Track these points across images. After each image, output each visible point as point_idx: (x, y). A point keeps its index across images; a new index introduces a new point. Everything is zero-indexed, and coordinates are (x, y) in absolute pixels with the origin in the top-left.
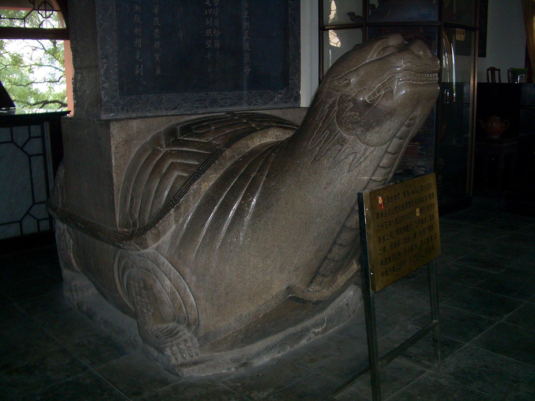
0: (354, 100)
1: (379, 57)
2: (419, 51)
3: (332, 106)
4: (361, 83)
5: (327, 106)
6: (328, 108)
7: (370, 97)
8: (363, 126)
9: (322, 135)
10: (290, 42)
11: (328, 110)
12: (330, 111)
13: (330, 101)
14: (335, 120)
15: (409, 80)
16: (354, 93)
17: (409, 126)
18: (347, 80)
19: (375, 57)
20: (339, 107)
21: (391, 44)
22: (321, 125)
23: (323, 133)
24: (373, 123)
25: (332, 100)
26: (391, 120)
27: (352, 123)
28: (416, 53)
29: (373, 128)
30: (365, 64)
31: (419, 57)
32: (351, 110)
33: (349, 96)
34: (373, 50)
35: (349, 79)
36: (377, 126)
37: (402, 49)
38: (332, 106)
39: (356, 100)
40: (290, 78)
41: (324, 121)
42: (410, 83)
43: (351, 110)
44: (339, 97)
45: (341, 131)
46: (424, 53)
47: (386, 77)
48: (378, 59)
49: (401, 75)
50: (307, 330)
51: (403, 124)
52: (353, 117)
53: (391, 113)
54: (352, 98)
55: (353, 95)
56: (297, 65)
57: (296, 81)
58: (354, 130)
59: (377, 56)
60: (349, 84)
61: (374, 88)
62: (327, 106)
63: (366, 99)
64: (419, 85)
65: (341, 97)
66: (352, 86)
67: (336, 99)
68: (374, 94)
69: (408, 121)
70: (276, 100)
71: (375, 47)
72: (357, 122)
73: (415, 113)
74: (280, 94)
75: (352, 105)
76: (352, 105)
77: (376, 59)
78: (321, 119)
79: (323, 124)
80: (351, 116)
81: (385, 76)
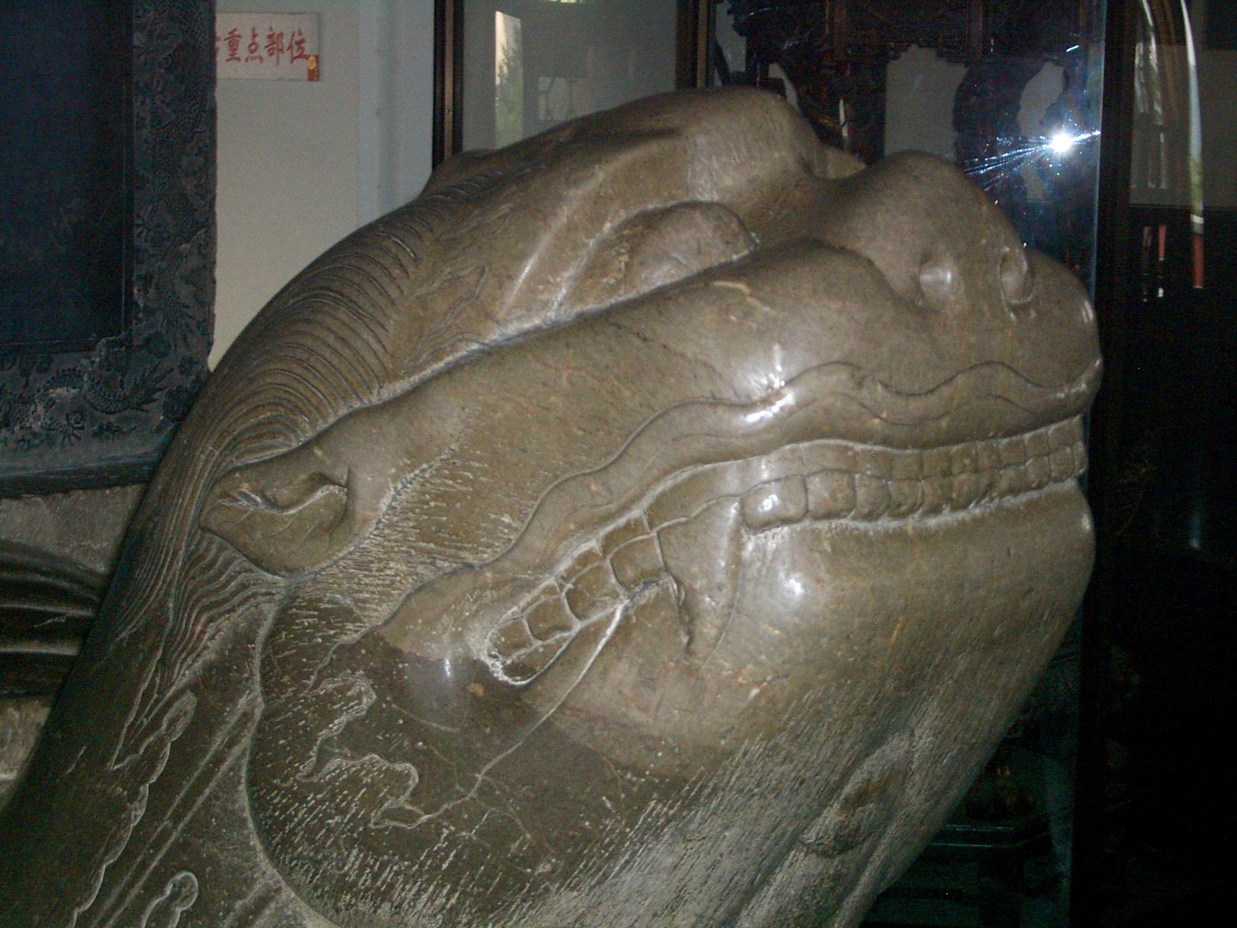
0: (383, 660)
1: (591, 306)
2: (926, 259)
3: (219, 682)
4: (442, 526)
5: (184, 675)
6: (193, 687)
7: (509, 641)
8: (453, 875)
9: (142, 901)
10: (138, 39)
11: (189, 702)
12: (203, 723)
13: (212, 641)
14: (243, 799)
15: (829, 515)
16: (385, 596)
17: (844, 842)
18: (323, 479)
19: (558, 304)
20: (267, 691)
21: (707, 195)
22: (138, 812)
23: (155, 887)
24: (533, 858)
25: (225, 623)
26: (683, 835)
27: (368, 842)
28: (898, 278)
29: (537, 894)
30: (472, 362)
31: (917, 308)
32: (357, 738)
33: (347, 615)
34: (546, 240)
35: (341, 473)
36: (564, 876)
37: (787, 241)
38: (219, 682)
39: (395, 653)
40: (141, 270)
41: (163, 790)
42: (843, 534)
43: (357, 738)
44: (270, 611)
45: (288, 893)
46: (966, 274)
47: (639, 482)
48: (586, 323)
49: (765, 469)
50: (818, 755)
51: (794, 841)
52: (373, 800)
53: (680, 786)
54: (372, 639)
55: (378, 613)
56: (189, 186)
57: (185, 292)
58: (383, 895)
59: (577, 294)
60: (342, 519)
61: (546, 565)
62: (184, 675)
63: (481, 644)
64: (926, 537)
65: (284, 620)
66: (368, 538)
67: (255, 622)
68: (544, 620)
69: (831, 816)
70: (37, 418)
71: (564, 215)
72: (410, 844)
73: (894, 749)
74: (69, 377)
75: (363, 694)
76: (363, 694)
77: (569, 313)
78: (140, 773)
79: (154, 812)
80: (354, 782)
81: (627, 478)
